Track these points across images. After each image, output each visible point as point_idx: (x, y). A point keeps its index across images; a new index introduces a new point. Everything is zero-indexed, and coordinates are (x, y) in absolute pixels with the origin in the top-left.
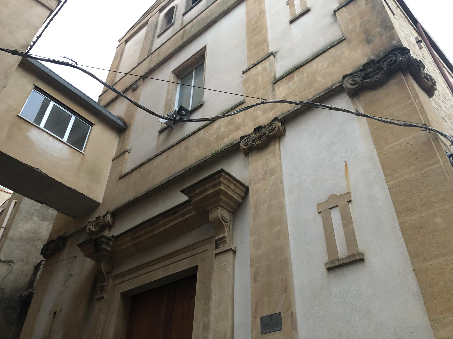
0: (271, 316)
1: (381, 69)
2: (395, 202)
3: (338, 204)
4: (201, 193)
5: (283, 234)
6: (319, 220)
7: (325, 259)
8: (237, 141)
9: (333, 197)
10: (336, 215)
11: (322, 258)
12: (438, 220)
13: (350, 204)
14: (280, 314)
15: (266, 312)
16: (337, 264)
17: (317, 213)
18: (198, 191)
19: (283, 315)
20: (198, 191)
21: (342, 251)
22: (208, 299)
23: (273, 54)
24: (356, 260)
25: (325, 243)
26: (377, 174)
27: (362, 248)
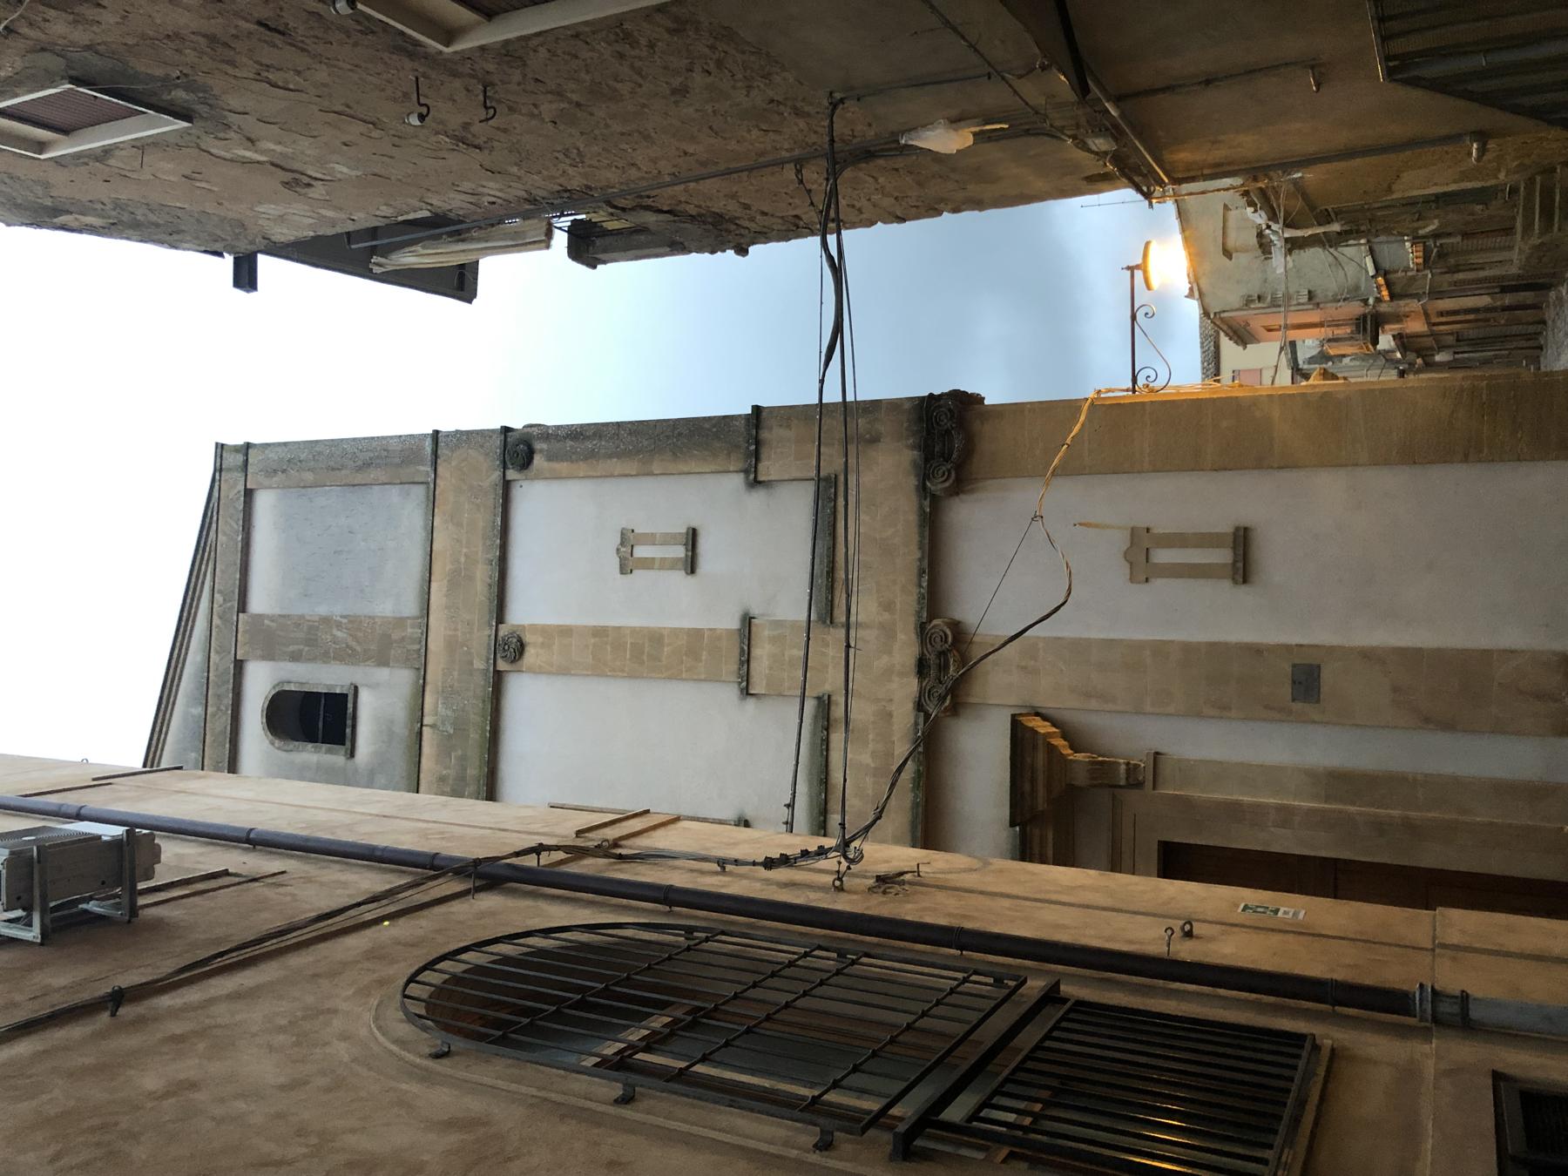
0: (1294, 682)
1: (948, 432)
2: (1180, 469)
3: (1142, 555)
4: (1033, 781)
5: (1160, 649)
6: (1159, 583)
7: (1226, 584)
8: (921, 720)
9: (1127, 555)
10: (1162, 556)
11: (1224, 589)
12: (1225, 424)
13: (1155, 531)
14: (1294, 666)
15: (1286, 690)
16: (1240, 565)
17: (1146, 586)
18: (1027, 787)
19: (1297, 661)
20: (1027, 787)
21: (1223, 556)
22: (1234, 811)
23: (748, 620)
24: (1242, 541)
25: (1202, 581)
26: (1119, 485)
27: (1225, 527)
